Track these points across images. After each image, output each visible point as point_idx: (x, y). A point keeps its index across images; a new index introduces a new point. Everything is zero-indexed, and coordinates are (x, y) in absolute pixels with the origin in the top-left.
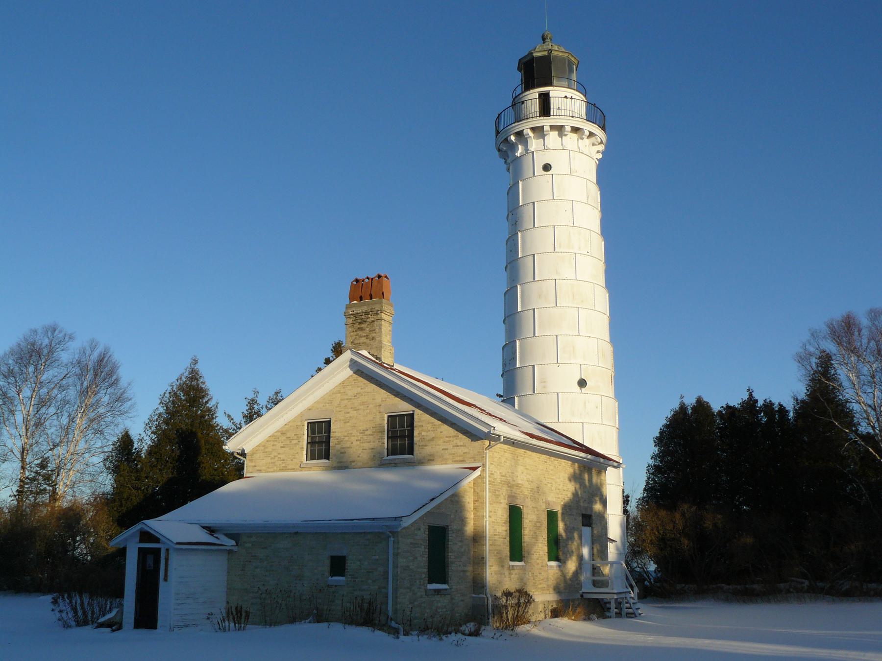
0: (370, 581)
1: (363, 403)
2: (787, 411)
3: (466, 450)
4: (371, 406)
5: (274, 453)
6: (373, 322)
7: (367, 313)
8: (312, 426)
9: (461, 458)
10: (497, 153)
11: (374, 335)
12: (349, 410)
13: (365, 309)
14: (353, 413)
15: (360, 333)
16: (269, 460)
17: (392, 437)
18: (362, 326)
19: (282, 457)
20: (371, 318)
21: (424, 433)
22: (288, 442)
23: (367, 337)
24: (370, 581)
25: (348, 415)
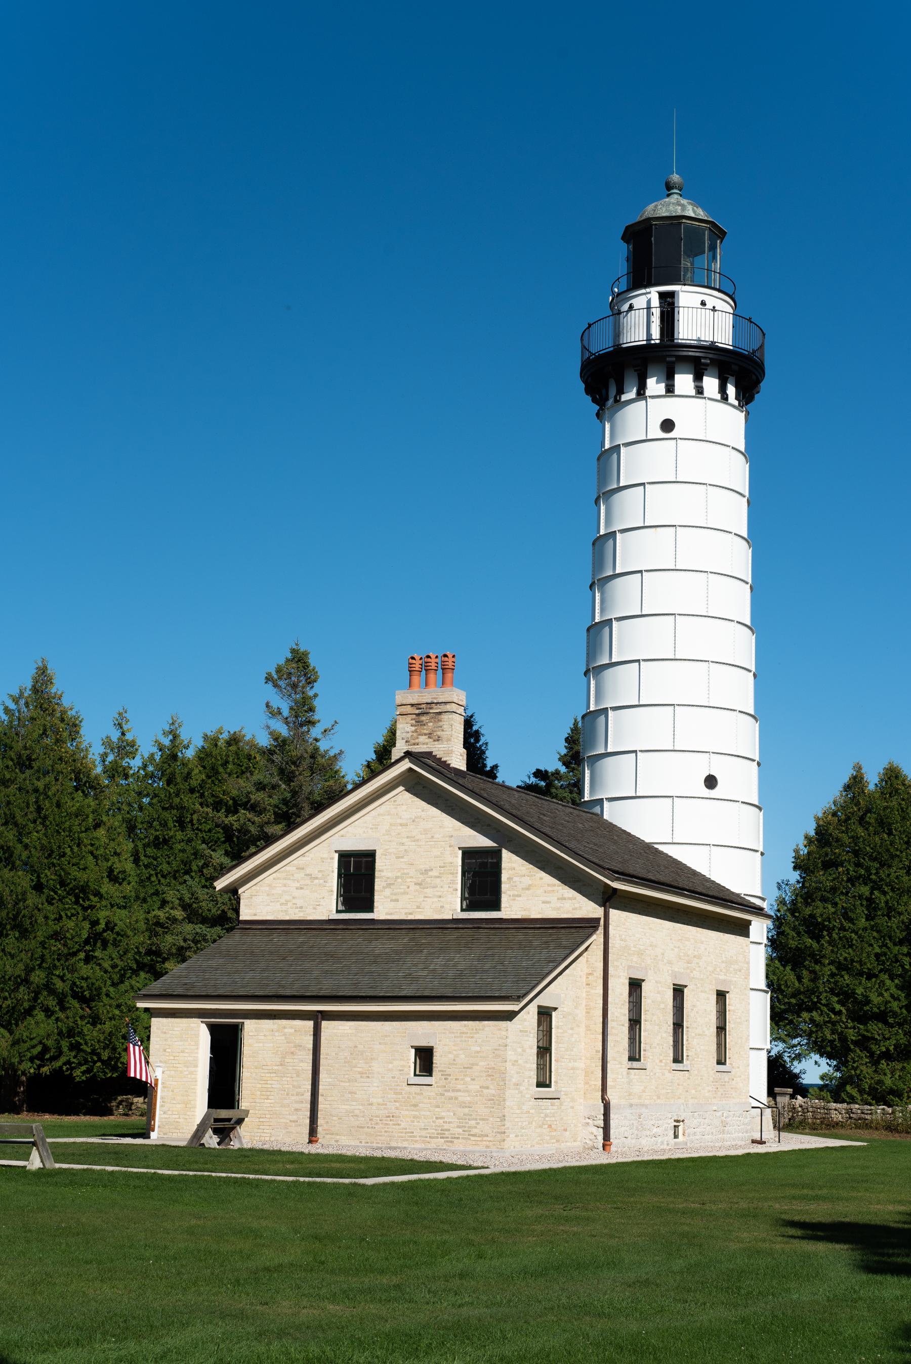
6: (440, 713)
12: (404, 840)
19: (300, 902)
21: (515, 879)
25: (402, 848)
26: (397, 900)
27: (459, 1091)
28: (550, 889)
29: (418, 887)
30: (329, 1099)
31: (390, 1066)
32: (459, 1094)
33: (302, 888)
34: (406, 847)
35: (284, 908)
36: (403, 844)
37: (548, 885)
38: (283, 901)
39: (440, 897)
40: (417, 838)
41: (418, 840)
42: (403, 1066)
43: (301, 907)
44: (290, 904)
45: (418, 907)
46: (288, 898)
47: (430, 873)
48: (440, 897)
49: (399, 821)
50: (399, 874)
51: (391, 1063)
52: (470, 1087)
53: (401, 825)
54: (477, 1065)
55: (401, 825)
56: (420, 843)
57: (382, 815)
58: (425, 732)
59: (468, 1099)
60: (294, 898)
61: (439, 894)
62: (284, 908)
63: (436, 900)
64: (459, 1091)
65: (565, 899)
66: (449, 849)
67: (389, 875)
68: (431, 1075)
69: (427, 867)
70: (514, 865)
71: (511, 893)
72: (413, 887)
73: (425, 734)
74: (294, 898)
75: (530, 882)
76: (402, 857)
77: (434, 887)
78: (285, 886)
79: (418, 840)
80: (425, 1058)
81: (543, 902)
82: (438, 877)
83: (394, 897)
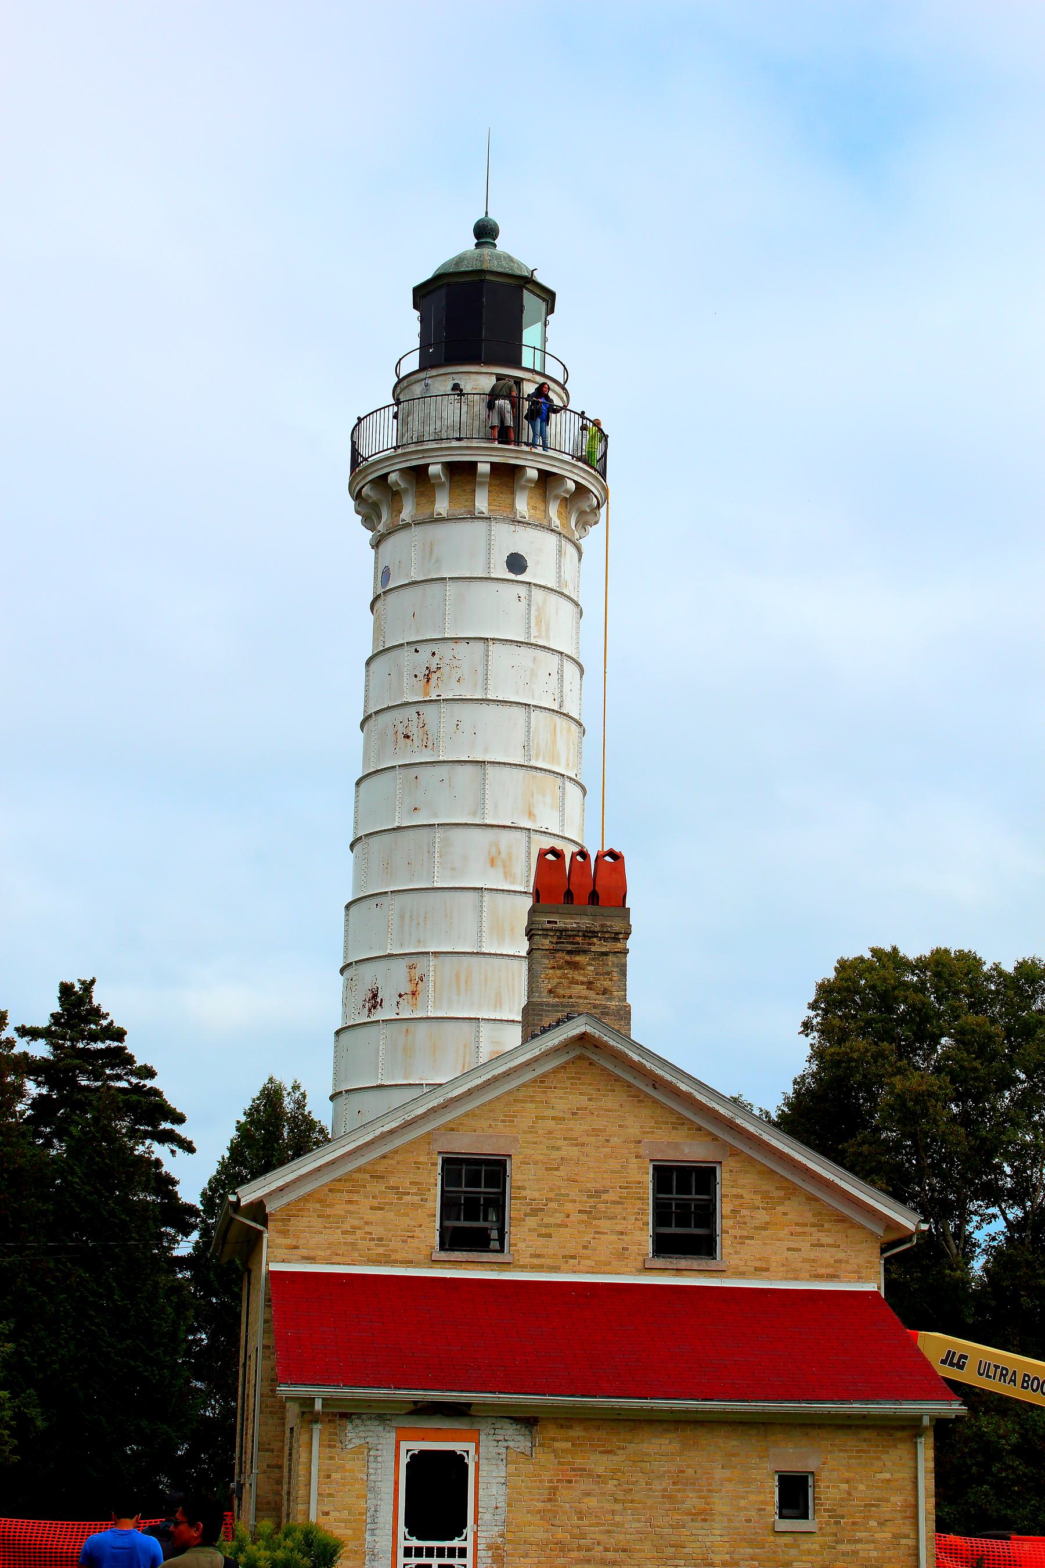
0: (873, 1523)
1: (596, 1132)
2: (154, 1113)
3: (841, 1255)
4: (615, 1140)
5: (352, 1221)
6: (605, 954)
7: (589, 934)
8: (456, 1168)
9: (830, 1271)
10: (351, 503)
11: (607, 983)
12: (560, 1143)
13: (585, 922)
14: (570, 1151)
15: (571, 973)
16: (337, 1236)
17: (707, 1215)
18: (577, 958)
19: (377, 1231)
20: (599, 946)
21: (744, 1212)
22: (392, 1197)
23: (590, 985)
24: (873, 1523)
25: (555, 1154)
26: (550, 1236)
27: (859, 1541)
28: (798, 1229)
29: (585, 1217)
30: (636, 1555)
31: (742, 1503)
32: (859, 1546)
33: (382, 1209)
34: (563, 1153)
35: (350, 1238)
36: (558, 1149)
37: (796, 1224)
38: (347, 1227)
39: (622, 1233)
40: (580, 1140)
41: (583, 1145)
42: (764, 1502)
43: (381, 1239)
44: (359, 1233)
45: (585, 1247)
46: (357, 1223)
47: (604, 1197)
48: (622, 1233)
49: (550, 1113)
50: (552, 1195)
51: (744, 1498)
52: (878, 1536)
53: (553, 1118)
54: (888, 1501)
55: (553, 1118)
56: (586, 1149)
57: (522, 1101)
58: (581, 978)
59: (874, 1554)
60: (366, 1223)
61: (619, 1228)
62: (350, 1238)
63: (614, 1237)
64: (859, 1541)
65: (822, 1246)
66: (634, 1160)
67: (536, 1195)
68: (805, 1516)
69: (598, 1186)
70: (740, 1191)
71: (738, 1232)
72: (575, 1217)
73: (582, 983)
74: (366, 1223)
75: (767, 1219)
76: (557, 1169)
77: (611, 1218)
78: (350, 1202)
79: (583, 1145)
80: (794, 1494)
81: (789, 1249)
82: (618, 1203)
83: (544, 1231)
